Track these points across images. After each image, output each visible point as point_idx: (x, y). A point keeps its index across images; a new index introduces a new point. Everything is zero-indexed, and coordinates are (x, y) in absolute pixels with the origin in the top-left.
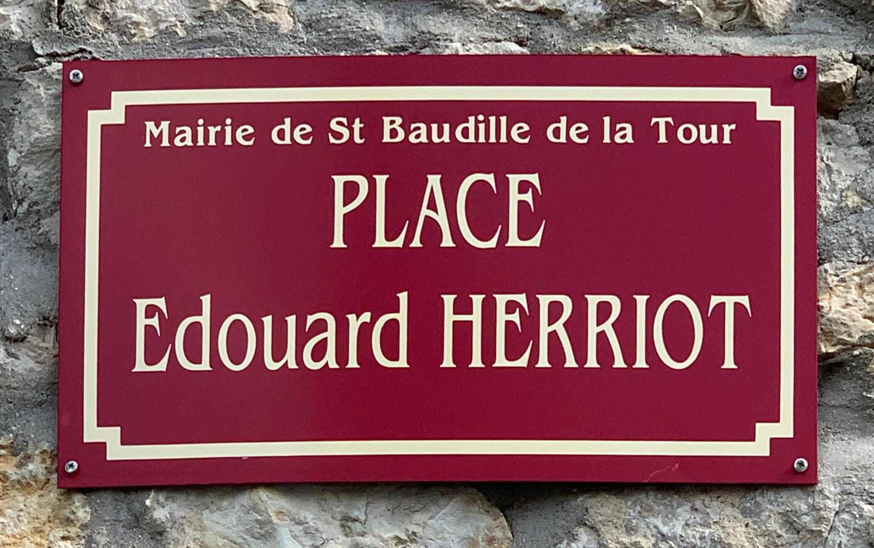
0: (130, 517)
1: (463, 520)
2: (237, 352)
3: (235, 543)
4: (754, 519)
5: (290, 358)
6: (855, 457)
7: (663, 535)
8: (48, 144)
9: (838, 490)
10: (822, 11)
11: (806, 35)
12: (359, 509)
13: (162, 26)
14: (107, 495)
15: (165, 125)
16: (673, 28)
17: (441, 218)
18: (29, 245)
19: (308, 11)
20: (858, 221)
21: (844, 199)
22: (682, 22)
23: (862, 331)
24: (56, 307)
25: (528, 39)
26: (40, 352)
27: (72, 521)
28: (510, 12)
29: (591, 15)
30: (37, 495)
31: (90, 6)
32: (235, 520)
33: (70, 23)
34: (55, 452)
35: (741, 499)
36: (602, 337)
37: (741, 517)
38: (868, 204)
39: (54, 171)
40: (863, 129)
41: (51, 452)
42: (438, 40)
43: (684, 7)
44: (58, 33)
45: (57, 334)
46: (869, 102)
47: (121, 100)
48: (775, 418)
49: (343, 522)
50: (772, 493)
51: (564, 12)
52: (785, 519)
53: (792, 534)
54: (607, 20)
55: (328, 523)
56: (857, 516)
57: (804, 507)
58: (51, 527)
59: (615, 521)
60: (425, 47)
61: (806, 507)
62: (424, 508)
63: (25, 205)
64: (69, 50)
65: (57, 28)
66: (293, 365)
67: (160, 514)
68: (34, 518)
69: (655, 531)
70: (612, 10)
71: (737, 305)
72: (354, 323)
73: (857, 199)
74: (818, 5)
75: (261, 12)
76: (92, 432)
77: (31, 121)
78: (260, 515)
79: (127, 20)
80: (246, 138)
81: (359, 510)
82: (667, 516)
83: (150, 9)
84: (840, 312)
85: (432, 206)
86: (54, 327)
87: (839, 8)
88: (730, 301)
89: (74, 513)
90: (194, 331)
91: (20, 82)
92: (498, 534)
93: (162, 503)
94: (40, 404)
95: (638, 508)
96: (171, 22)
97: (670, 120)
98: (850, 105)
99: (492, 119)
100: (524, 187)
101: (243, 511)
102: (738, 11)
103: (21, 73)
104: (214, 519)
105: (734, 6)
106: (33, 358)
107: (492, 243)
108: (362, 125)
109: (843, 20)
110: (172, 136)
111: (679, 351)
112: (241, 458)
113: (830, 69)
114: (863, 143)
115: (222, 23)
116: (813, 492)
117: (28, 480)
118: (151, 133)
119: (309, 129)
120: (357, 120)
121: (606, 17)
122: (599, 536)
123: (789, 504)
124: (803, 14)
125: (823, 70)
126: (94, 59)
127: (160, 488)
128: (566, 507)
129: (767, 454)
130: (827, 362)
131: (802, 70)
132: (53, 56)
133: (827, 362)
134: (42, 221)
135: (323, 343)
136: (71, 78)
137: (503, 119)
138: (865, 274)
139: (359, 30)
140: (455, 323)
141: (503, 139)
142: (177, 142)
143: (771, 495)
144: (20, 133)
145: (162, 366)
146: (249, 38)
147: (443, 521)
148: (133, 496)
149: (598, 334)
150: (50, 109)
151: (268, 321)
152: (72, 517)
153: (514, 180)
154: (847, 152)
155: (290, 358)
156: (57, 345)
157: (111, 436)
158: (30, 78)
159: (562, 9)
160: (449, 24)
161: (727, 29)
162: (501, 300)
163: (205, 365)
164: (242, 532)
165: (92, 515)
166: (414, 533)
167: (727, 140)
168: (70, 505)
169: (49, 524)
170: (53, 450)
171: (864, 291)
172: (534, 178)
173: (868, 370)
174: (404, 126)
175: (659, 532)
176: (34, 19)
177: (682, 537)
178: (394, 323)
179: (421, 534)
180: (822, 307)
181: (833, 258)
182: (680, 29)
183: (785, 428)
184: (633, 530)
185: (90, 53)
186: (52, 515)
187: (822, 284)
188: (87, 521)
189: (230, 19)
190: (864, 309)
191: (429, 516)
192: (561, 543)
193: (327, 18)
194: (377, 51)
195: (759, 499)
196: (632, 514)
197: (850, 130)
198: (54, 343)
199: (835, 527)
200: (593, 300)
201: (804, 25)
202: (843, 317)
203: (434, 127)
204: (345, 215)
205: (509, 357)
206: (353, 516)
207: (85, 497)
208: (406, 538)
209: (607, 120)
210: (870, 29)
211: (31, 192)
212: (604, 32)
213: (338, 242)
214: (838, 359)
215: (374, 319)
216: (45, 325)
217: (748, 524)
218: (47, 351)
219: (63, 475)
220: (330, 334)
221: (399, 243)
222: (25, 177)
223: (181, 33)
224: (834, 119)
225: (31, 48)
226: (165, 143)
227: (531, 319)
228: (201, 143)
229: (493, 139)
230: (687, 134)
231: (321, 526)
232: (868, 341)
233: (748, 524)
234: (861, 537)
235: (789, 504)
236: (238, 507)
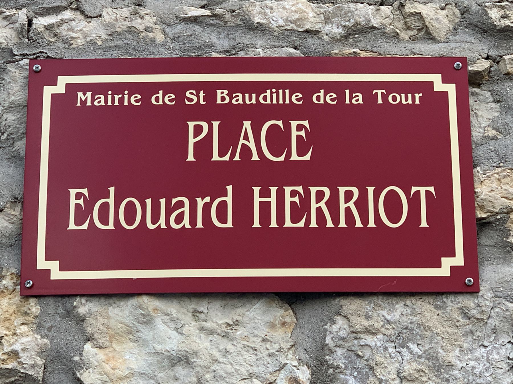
0: (64, 311)
1: (267, 312)
2: (130, 217)
3: (128, 326)
4: (443, 311)
5: (162, 223)
6: (501, 275)
7: (388, 321)
8: (20, 103)
9: (493, 295)
10: (467, 30)
11: (459, 43)
12: (203, 306)
13: (88, 39)
14: (49, 299)
15: (89, 94)
16: (383, 40)
17: (252, 145)
18: (7, 157)
19: (173, 31)
20: (495, 144)
21: (486, 132)
22: (388, 37)
23: (502, 205)
24: (22, 193)
25: (300, 46)
26: (12, 217)
27: (28, 314)
28: (289, 32)
29: (336, 34)
30: (7, 298)
31: (46, 29)
32: (128, 313)
33: (35, 37)
34: (19, 274)
35: (434, 299)
36: (348, 210)
37: (434, 310)
38: (501, 134)
39: (23, 117)
40: (495, 94)
41: (17, 274)
42: (248, 47)
43: (389, 29)
44: (28, 43)
45: (22, 207)
46: (498, 80)
47: (63, 81)
48: (453, 254)
49: (193, 314)
50: (453, 297)
51: (320, 32)
52: (461, 311)
53: (466, 319)
54: (345, 36)
55: (185, 314)
56: (505, 310)
57: (472, 305)
58: (15, 317)
59: (358, 313)
60: (241, 51)
61: (473, 305)
62: (243, 305)
63: (6, 135)
64: (34, 52)
65: (27, 40)
66: (163, 226)
67: (82, 310)
68: (5, 312)
69: (383, 318)
70: (348, 31)
71: (427, 192)
72: (200, 203)
73: (494, 132)
74: (465, 27)
75: (145, 32)
76: (42, 264)
77: (10, 91)
78: (143, 311)
79: (68, 36)
80: (136, 101)
81: (204, 307)
82: (390, 310)
83: (81, 30)
84: (488, 195)
85: (246, 138)
86: (20, 203)
87: (477, 29)
88: (423, 190)
89: (30, 309)
90: (105, 207)
91: (4, 70)
92: (288, 320)
93: (84, 304)
94: (11, 246)
95: (372, 305)
96: (93, 37)
97: (384, 91)
98: (486, 81)
99: (281, 91)
100: (300, 128)
101: (133, 308)
102: (419, 30)
103: (5, 64)
104: (116, 312)
105: (417, 28)
106: (7, 221)
107: (282, 158)
108: (204, 95)
109: (480, 36)
110: (93, 100)
111: (394, 217)
112: (132, 279)
113: (475, 63)
114: (495, 101)
115: (123, 38)
116: (477, 296)
117: (2, 290)
118: (81, 98)
119: (173, 96)
120: (202, 92)
121: (344, 35)
122: (349, 321)
123: (463, 303)
124: (456, 31)
125: (470, 64)
126: (48, 57)
127: (82, 296)
128: (329, 305)
129: (449, 275)
130: (481, 222)
131: (459, 64)
132: (24, 56)
133: (481, 222)
134: (16, 144)
135: (182, 213)
136: (34, 68)
137: (287, 91)
138: (501, 173)
139: (202, 42)
140: (260, 202)
141: (287, 102)
142: (96, 103)
143: (452, 298)
144: (4, 96)
145: (85, 226)
146: (139, 46)
147: (254, 313)
148: (66, 299)
149: (346, 208)
150: (22, 84)
151: (149, 202)
152: (29, 312)
153: (294, 124)
154: (486, 106)
155: (162, 223)
156: (22, 214)
157: (53, 266)
158: (10, 67)
159: (319, 30)
160: (255, 39)
161: (414, 39)
162: (288, 190)
163: (111, 226)
164: (132, 320)
165: (41, 310)
166: (237, 321)
167: (417, 102)
168: (27, 304)
169: (14, 315)
170: (18, 273)
171: (501, 182)
172: (306, 123)
173: (506, 226)
174: (230, 95)
175: (386, 319)
176: (13, 36)
177: (400, 322)
178: (225, 203)
179: (242, 321)
180: (477, 192)
181: (482, 164)
182: (387, 40)
183: (459, 260)
184: (370, 318)
185: (46, 53)
186: (16, 310)
187: (477, 179)
188: (37, 314)
189: (129, 36)
190: (501, 193)
191: (246, 310)
192: (326, 325)
193: (184, 35)
194: (213, 53)
195: (445, 300)
196: (369, 309)
197: (488, 94)
198: (20, 212)
199: (492, 317)
200: (342, 190)
201: (458, 37)
202: (490, 198)
203: (247, 95)
204: (194, 143)
205: (293, 221)
206: (200, 310)
207: (37, 300)
208: (232, 323)
209: (347, 91)
210: (496, 41)
211: (9, 128)
212: (343, 42)
213: (191, 158)
214: (488, 220)
215: (212, 201)
216: (15, 202)
217: (439, 314)
218: (16, 217)
219: (23, 288)
220: (186, 209)
221: (227, 158)
222: (6, 120)
223: (99, 43)
224: (478, 88)
225: (11, 51)
226: (89, 104)
227: (306, 200)
228: (110, 103)
229: (281, 102)
230: (394, 99)
231: (180, 316)
232: (505, 210)
233: (439, 314)
234: (507, 321)
235: (463, 303)
236: (130, 306)
